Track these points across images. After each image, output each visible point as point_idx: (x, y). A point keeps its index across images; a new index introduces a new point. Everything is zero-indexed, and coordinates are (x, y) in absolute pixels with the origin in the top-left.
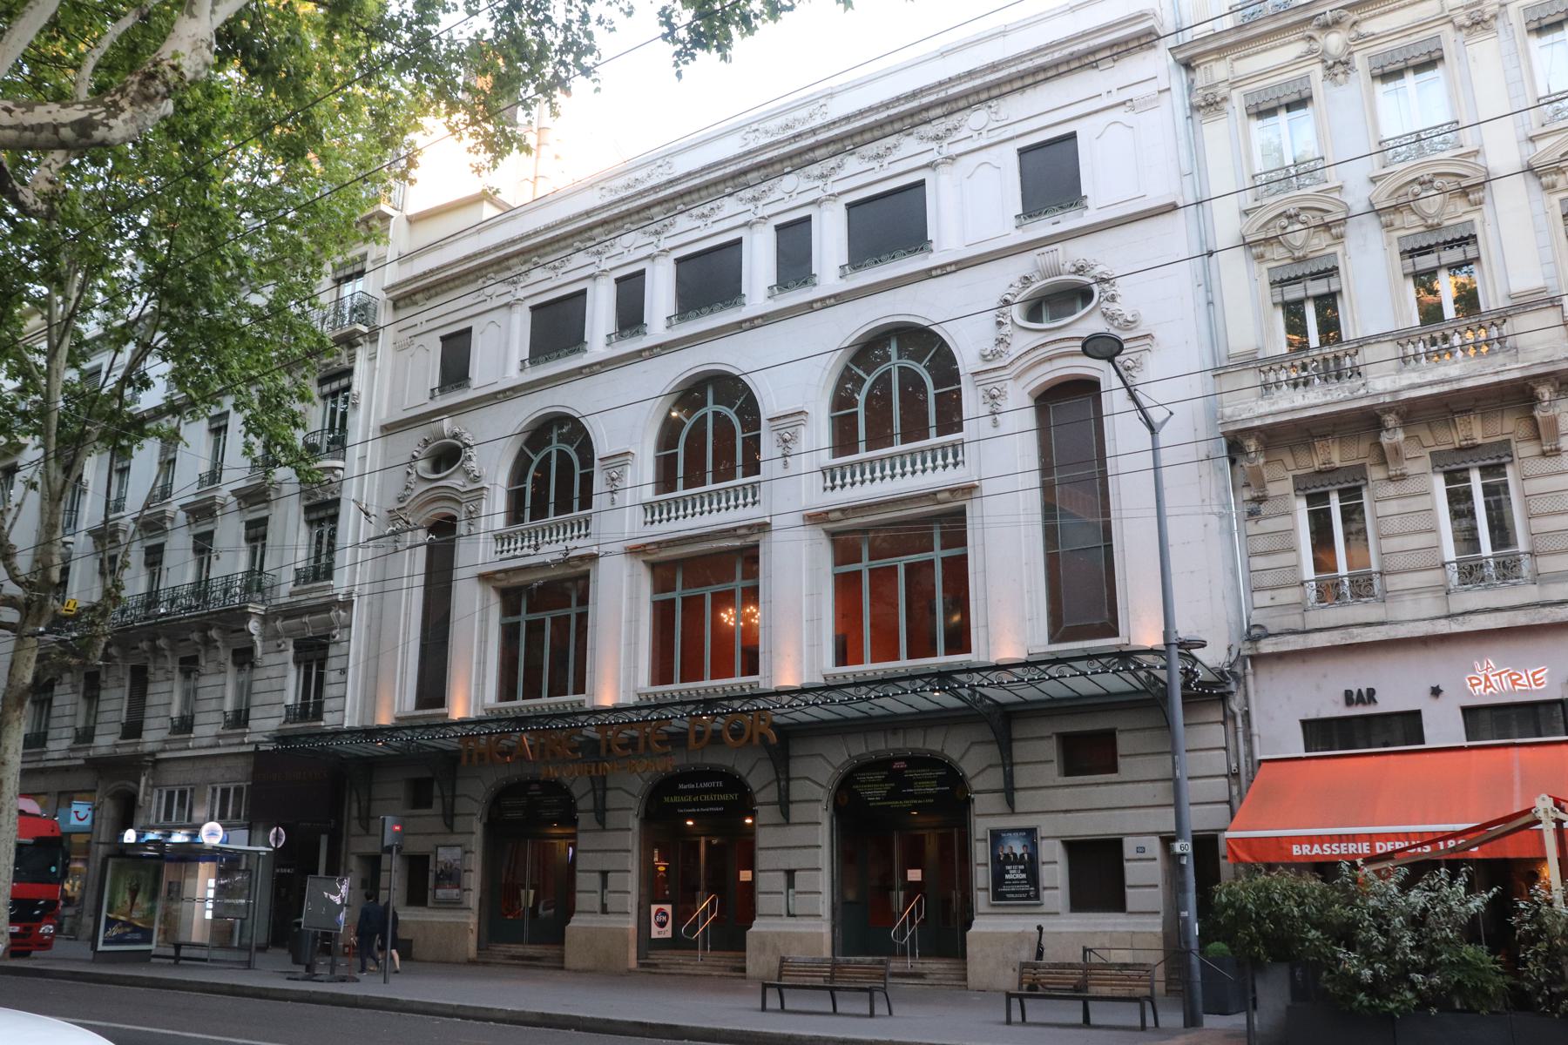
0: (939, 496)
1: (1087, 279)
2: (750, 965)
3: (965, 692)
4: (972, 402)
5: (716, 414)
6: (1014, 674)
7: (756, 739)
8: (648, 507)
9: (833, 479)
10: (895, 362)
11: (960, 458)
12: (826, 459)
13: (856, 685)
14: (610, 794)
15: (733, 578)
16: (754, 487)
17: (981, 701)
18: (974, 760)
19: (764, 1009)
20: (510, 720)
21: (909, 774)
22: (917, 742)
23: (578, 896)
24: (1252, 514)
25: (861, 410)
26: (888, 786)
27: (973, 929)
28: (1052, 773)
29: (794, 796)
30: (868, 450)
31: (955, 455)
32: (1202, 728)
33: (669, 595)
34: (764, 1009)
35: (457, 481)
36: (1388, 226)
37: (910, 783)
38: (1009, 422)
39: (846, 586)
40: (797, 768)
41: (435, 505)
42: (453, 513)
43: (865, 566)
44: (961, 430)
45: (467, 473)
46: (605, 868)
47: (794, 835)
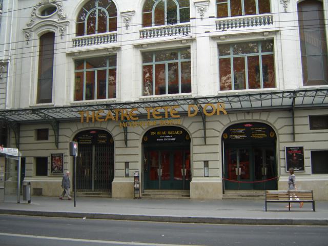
0: (143, 46)
2: (192, 194)
3: (42, 115)
4: (120, 22)
5: (99, 10)
6: (324, 93)
8: (75, 41)
9: (76, 43)
11: (189, 30)
12: (74, 37)
13: (80, 106)
14: (60, 137)
15: (83, 68)
16: (115, 36)
17: (48, 117)
18: (278, 124)
19: (266, 211)
20: (105, 105)
22: (256, 118)
25: (153, 12)
27: (192, 181)
28: (33, 140)
29: (60, 140)
30: (98, 33)
31: (114, 38)
32: (211, 123)
33: (111, 68)
34: (266, 211)
35: (54, 18)
38: (32, 43)
39: (78, 77)
40: (61, 132)
41: (45, 27)
42: (54, 31)
43: (154, 63)
44: (116, 30)
45: (59, 16)
47: (128, 151)
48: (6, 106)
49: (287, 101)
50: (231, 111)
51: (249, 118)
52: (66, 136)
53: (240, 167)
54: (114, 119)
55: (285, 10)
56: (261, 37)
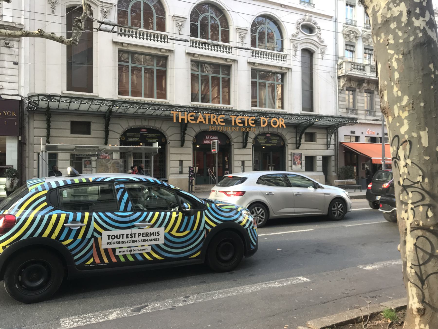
1: (315, 26)
7: (280, 126)
10: (210, 13)
11: (230, 51)
21: (270, 137)
22: (152, 124)
23: (322, 165)
24: (340, 92)
26: (266, 140)
36: (364, 42)
37: (271, 140)
46: (182, 160)
48: (20, 87)
49: (104, 109)
50: (134, 116)
51: (145, 124)
52: (115, 132)
53: (273, 166)
54: (204, 122)
55: (53, 12)
56: (159, 53)
